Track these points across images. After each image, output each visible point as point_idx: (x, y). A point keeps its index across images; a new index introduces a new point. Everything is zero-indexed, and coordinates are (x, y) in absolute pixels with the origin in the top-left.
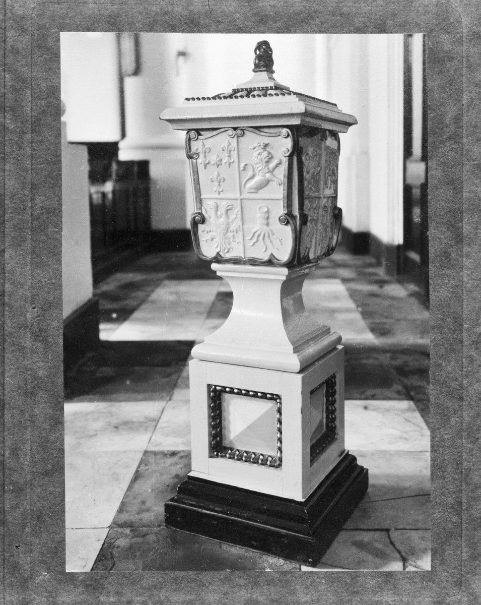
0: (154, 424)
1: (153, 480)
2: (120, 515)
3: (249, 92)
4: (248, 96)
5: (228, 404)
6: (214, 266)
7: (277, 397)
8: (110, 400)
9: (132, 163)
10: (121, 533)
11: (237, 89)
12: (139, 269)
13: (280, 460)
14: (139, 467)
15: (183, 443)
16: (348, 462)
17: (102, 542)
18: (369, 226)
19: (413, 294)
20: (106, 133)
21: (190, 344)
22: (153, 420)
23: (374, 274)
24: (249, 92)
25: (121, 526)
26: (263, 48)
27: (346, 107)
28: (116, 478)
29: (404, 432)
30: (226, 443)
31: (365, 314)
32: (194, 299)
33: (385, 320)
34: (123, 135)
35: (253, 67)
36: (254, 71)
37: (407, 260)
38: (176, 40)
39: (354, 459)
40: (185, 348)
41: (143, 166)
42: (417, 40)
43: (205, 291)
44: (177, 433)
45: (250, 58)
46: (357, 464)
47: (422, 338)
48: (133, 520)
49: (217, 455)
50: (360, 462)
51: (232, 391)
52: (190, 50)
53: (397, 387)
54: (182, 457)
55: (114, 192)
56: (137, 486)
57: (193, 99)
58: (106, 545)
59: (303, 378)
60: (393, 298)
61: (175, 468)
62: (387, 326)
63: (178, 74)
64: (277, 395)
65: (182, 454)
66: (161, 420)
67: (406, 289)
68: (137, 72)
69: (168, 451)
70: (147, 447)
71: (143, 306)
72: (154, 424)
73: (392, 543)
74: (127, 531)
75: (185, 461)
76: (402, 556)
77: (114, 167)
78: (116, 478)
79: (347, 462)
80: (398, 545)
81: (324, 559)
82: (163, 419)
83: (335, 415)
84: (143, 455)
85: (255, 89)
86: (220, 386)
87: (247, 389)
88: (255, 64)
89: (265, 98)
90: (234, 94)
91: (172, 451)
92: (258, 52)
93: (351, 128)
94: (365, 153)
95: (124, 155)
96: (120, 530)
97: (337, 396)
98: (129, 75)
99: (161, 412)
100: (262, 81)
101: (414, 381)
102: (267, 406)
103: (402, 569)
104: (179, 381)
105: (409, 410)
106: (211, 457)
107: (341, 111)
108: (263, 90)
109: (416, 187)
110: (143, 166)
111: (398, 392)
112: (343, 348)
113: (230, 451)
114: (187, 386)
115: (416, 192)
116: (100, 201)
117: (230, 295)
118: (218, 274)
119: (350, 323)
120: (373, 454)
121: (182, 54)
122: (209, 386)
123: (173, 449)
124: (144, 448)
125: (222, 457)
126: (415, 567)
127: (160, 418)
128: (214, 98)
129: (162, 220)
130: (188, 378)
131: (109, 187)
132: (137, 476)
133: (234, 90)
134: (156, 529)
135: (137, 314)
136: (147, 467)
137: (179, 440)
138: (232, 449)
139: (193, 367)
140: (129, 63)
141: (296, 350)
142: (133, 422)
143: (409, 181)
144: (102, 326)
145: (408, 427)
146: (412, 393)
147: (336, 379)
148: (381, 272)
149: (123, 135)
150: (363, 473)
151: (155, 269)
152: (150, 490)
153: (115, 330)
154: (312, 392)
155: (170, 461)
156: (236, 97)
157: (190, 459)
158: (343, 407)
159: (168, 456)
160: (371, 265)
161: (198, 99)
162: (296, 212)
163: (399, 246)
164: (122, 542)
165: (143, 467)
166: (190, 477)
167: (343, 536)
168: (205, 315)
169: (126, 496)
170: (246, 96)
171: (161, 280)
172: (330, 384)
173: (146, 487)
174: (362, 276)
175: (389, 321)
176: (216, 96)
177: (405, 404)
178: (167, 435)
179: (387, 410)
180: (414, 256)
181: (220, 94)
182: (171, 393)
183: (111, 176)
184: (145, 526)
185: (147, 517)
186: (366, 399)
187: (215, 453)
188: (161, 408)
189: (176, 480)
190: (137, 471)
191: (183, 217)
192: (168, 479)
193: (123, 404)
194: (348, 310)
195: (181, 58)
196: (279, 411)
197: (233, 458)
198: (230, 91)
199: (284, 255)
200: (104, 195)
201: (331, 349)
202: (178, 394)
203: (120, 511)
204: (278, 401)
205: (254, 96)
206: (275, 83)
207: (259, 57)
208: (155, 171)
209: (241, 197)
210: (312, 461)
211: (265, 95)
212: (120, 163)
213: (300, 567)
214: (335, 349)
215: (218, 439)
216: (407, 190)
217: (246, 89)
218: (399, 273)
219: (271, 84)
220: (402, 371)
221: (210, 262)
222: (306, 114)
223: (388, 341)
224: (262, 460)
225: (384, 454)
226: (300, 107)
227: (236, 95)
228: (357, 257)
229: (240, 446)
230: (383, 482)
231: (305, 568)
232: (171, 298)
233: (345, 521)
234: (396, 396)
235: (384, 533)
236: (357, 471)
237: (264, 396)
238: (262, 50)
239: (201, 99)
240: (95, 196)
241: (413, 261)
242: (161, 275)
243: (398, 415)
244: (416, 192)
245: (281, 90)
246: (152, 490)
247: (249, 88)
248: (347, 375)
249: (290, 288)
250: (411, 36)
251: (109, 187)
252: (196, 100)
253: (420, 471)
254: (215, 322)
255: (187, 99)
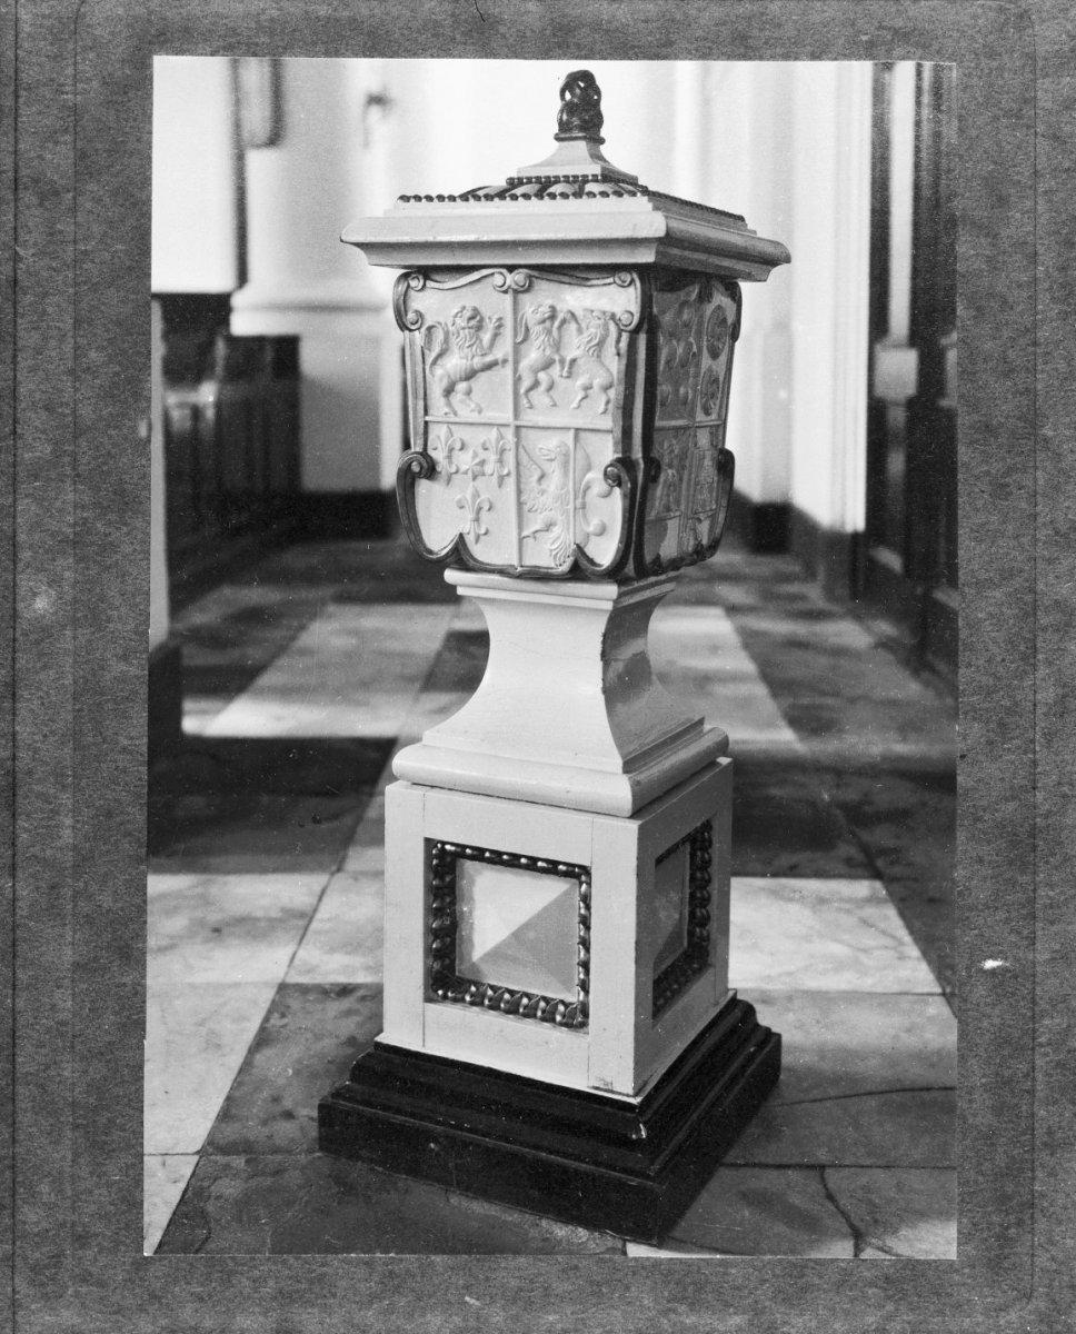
0: (302, 923)
1: (295, 1051)
2: (224, 1125)
3: (543, 187)
4: (539, 195)
5: (472, 883)
6: (451, 576)
7: (581, 871)
8: (205, 870)
9: (260, 341)
10: (227, 1166)
11: (518, 179)
12: (270, 579)
13: (585, 1014)
14: (266, 1019)
15: (368, 968)
16: (738, 1015)
17: (182, 1185)
18: (788, 487)
19: (884, 644)
20: (208, 276)
21: (385, 748)
22: (302, 915)
23: (803, 598)
24: (543, 187)
25: (225, 1150)
26: (579, 86)
27: (762, 227)
28: (214, 1044)
29: (859, 949)
30: (461, 969)
31: (778, 684)
32: (394, 645)
33: (819, 700)
34: (242, 277)
35: (556, 129)
36: (558, 138)
37: (874, 565)
38: (364, 73)
39: (749, 1010)
40: (373, 755)
41: (286, 349)
42: (904, 75)
43: (422, 630)
44: (352, 945)
45: (551, 107)
46: (758, 1025)
47: (905, 740)
48: (252, 1139)
49: (445, 997)
50: (765, 1018)
51: (479, 854)
52: (394, 93)
53: (846, 849)
54: (363, 998)
55: (219, 405)
56: (259, 1058)
57: (417, 198)
58: (190, 1193)
59: (641, 828)
60: (839, 652)
61: (335, 1027)
62: (825, 715)
63: (366, 144)
64: (581, 867)
65: (361, 992)
66: (319, 916)
67: (868, 630)
68: (274, 139)
69: (332, 984)
70: (287, 973)
71: (283, 661)
72: (302, 923)
73: (830, 1197)
74: (239, 1162)
75: (366, 1009)
76: (852, 1226)
77: (221, 348)
78: (214, 1044)
79: (738, 1013)
80: (843, 1202)
81: (677, 1233)
82: (322, 914)
83: (707, 911)
84: (278, 992)
85: (557, 180)
86: (452, 844)
87: (514, 851)
88: (561, 123)
89: (579, 201)
90: (510, 190)
91: (342, 984)
92: (568, 96)
93: (776, 271)
94: (782, 326)
95: (245, 322)
96: (221, 1159)
97: (714, 869)
98: (258, 146)
99: (317, 898)
100: (574, 155)
101: (882, 836)
102: (552, 889)
103: (852, 1253)
104: (360, 829)
105: (872, 900)
106: (428, 999)
107: (755, 232)
108: (574, 182)
109: (897, 404)
110: (286, 349)
111: (849, 862)
112: (730, 764)
113: (473, 989)
114: (378, 840)
115: (898, 417)
116: (188, 424)
117: (481, 639)
118: (460, 591)
119: (744, 704)
120: (790, 998)
121: (377, 100)
122: (429, 843)
123: (342, 979)
124: (280, 981)
125: (455, 1000)
126: (881, 1249)
127: (315, 910)
128: (465, 197)
129: (322, 471)
130: (381, 821)
131: (207, 394)
132: (263, 1039)
133: (511, 179)
134: (303, 1159)
135: (266, 679)
136: (285, 1021)
137: (357, 960)
138: (476, 984)
139: (397, 801)
140: (257, 117)
141: (628, 767)
142: (258, 919)
143: (880, 391)
144: (188, 705)
145: (869, 939)
146: (880, 863)
147: (713, 833)
148: (814, 593)
149: (242, 277)
150: (770, 1041)
151: (311, 578)
152: (291, 1071)
153: (218, 712)
154: (659, 861)
155: (335, 1007)
156: (515, 198)
157: (381, 1002)
158: (727, 895)
159: (332, 995)
160: (787, 578)
161: (429, 198)
162: (637, 454)
163: (855, 536)
164: (229, 1188)
165: (275, 1021)
166: (379, 1045)
167: (724, 1176)
168: (417, 685)
169: (238, 1083)
170: (536, 195)
171: (324, 603)
172: (699, 841)
173: (279, 1066)
174: (771, 597)
175: (830, 701)
176: (469, 193)
177: (862, 888)
178: (332, 950)
179: (822, 901)
180: (891, 559)
181: (480, 189)
182: (342, 854)
183: (212, 367)
184: (276, 1150)
185: (285, 1130)
186: (775, 875)
187: (440, 992)
188: (317, 889)
189: (350, 1051)
190: (262, 1029)
191: (374, 465)
192: (328, 1045)
193: (232, 879)
194: (735, 678)
195: (375, 111)
196: (586, 899)
197: (481, 1004)
198: (503, 184)
199: (605, 552)
200: (196, 412)
201: (706, 763)
202: (358, 859)
203: (225, 1115)
204: (583, 878)
205: (552, 196)
206: (603, 169)
207: (569, 108)
208: (313, 360)
209: (519, 423)
210: (657, 1011)
211: (578, 194)
212: (234, 341)
213: (624, 1246)
214: (713, 764)
215: (447, 961)
216: (877, 410)
217: (538, 179)
218: (854, 595)
219: (596, 169)
220: (860, 815)
221: (442, 564)
222: (668, 240)
223: (825, 747)
224: (543, 1012)
225: (823, 1000)
226: (653, 223)
227: (513, 192)
228: (760, 559)
229: (494, 977)
230: (806, 1059)
231: (636, 1251)
232: (341, 642)
233: (730, 1144)
234: (842, 868)
235: (813, 1173)
236: (759, 1036)
237: (552, 868)
238: (578, 91)
239: (436, 200)
240: (176, 414)
241: (887, 570)
242: (328, 591)
243: (848, 911)
244: (898, 417)
245: (618, 183)
246: (297, 1073)
247: (545, 177)
248: (737, 820)
249: (624, 625)
250: (888, 67)
251: (207, 394)
252: (424, 200)
253: (896, 1037)
254: (443, 698)
255: (404, 198)
